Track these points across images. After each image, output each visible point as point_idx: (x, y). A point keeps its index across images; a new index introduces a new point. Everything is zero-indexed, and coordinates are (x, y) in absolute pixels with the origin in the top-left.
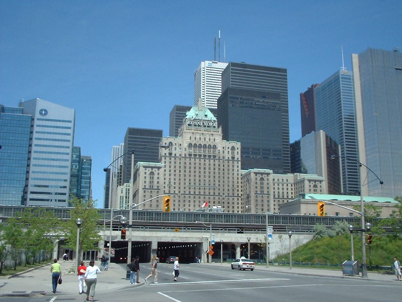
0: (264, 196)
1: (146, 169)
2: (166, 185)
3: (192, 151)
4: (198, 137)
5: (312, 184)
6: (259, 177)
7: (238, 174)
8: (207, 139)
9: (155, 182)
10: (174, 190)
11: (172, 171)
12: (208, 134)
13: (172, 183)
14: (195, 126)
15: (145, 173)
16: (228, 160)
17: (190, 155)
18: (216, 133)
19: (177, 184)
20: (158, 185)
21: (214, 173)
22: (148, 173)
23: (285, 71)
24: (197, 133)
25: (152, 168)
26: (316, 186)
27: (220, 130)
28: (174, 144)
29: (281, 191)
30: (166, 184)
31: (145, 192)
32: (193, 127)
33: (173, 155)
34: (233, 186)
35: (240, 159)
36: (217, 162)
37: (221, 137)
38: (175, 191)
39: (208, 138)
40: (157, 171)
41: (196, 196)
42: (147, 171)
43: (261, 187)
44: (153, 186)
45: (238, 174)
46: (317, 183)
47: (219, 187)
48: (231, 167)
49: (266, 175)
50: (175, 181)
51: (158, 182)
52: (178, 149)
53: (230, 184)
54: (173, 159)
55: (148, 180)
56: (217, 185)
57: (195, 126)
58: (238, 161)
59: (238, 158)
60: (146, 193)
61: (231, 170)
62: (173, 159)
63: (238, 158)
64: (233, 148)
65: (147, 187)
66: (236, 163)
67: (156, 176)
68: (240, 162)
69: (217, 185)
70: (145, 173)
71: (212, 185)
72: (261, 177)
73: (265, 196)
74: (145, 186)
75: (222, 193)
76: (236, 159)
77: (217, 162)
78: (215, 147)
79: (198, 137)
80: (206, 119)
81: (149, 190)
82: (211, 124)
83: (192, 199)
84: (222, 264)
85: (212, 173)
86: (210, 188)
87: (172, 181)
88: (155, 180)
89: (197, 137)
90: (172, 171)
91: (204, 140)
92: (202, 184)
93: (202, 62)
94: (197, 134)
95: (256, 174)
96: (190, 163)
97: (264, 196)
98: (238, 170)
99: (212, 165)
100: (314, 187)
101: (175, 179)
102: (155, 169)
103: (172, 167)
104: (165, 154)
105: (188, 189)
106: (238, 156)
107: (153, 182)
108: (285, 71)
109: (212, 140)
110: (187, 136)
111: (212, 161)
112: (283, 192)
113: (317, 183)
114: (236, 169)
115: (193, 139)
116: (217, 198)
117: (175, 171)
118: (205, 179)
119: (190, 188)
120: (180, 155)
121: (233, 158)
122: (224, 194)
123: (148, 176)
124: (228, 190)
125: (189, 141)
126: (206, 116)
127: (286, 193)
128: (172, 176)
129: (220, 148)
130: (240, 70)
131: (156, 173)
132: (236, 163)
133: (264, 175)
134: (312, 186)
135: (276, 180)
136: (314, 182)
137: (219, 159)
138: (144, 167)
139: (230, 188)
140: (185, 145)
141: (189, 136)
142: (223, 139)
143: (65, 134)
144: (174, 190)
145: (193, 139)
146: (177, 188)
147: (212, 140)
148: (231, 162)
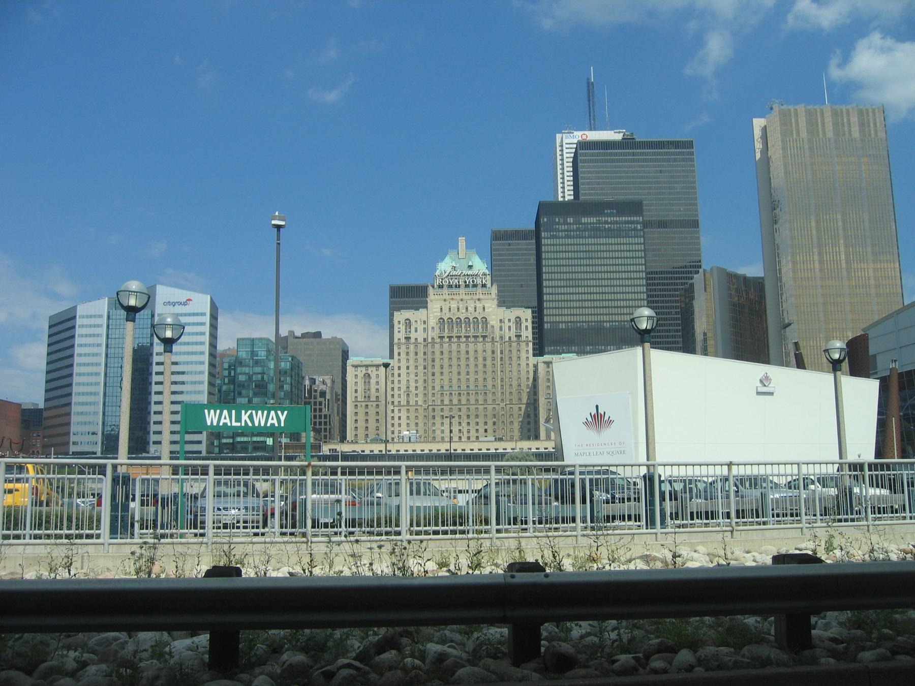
2: (402, 392)
4: (454, 305)
8: (471, 309)
9: (373, 390)
13: (412, 389)
14: (450, 286)
15: (356, 375)
16: (433, 342)
18: (486, 297)
19: (421, 389)
21: (485, 365)
22: (360, 375)
27: (494, 290)
28: (413, 321)
30: (402, 391)
33: (413, 340)
35: (530, 338)
37: (496, 302)
39: (473, 305)
40: (375, 372)
42: (358, 373)
54: (412, 347)
56: (490, 387)
62: (412, 347)
66: (523, 345)
67: (373, 381)
68: (531, 344)
69: (490, 387)
71: (481, 387)
76: (524, 338)
77: (489, 346)
78: (485, 321)
79: (454, 305)
80: (470, 272)
81: (364, 404)
85: (481, 367)
88: (373, 387)
92: (464, 387)
93: (754, 120)
97: (369, 404)
101: (416, 381)
109: (479, 310)
114: (523, 355)
115: (446, 310)
116: (481, 408)
123: (360, 381)
126: (470, 267)
128: (412, 376)
129: (493, 321)
130: (592, 155)
131: (373, 376)
132: (523, 345)
133: (370, 369)
139: (514, 390)
140: (433, 322)
143: (197, 334)
145: (446, 310)
146: (421, 396)
147: (479, 310)
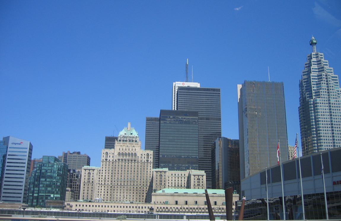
0: (158, 187)
1: (86, 171)
3: (121, 157)
4: (124, 148)
5: (197, 177)
6: (159, 174)
7: (150, 171)
8: (130, 150)
9: (91, 179)
10: (108, 183)
11: (107, 171)
12: (131, 146)
13: (107, 178)
15: (85, 173)
16: (144, 162)
17: (119, 160)
18: (137, 145)
19: (110, 179)
20: (93, 180)
23: (219, 90)
24: (124, 146)
25: (161, 172)
26: (199, 179)
28: (109, 153)
29: (180, 182)
31: (84, 185)
32: (122, 142)
33: (108, 160)
34: (147, 179)
36: (136, 164)
38: (108, 183)
39: (131, 148)
41: (122, 186)
43: (160, 181)
44: (89, 181)
45: (150, 171)
46: (200, 176)
47: (137, 181)
48: (146, 167)
49: (164, 173)
50: (109, 177)
51: (93, 176)
52: (111, 156)
53: (176, 179)
54: (108, 163)
55: (87, 177)
56: (136, 179)
57: (123, 141)
58: (151, 163)
59: (151, 161)
60: (85, 185)
61: (146, 169)
62: (108, 163)
63: (151, 161)
64: (148, 155)
65: (86, 182)
66: (149, 164)
67: (91, 175)
68: (152, 164)
69: (136, 179)
70: (85, 173)
71: (132, 179)
72: (160, 174)
73: (162, 187)
74: (85, 181)
75: (139, 184)
76: (149, 162)
77: (136, 164)
78: (135, 154)
79: (124, 148)
80: (131, 136)
82: (134, 139)
83: (119, 188)
84: (51, 209)
86: (121, 181)
87: (107, 177)
89: (124, 148)
90: (107, 171)
91: (128, 150)
92: (123, 179)
94: (124, 147)
95: (157, 172)
96: (119, 165)
98: (150, 169)
99: (130, 166)
100: (198, 179)
101: (108, 176)
102: (201, 176)
103: (107, 168)
104: (103, 160)
105: (117, 182)
106: (151, 160)
107: (89, 179)
108: (219, 90)
110: (117, 148)
111: (133, 164)
112: (181, 183)
113: (200, 176)
114: (149, 168)
115: (121, 150)
117: (109, 171)
118: (128, 175)
119: (124, 182)
120: (113, 160)
121: (148, 161)
122: (140, 185)
124: (143, 182)
125: (119, 151)
126: (132, 134)
127: (184, 183)
129: (139, 155)
131: (92, 173)
132: (149, 164)
134: (196, 179)
135: (177, 175)
136: (197, 176)
137: (138, 162)
138: (156, 171)
140: (116, 154)
141: (119, 148)
142: (145, 150)
144: (108, 183)
145: (121, 150)
146: (110, 181)
148: (104, 163)
